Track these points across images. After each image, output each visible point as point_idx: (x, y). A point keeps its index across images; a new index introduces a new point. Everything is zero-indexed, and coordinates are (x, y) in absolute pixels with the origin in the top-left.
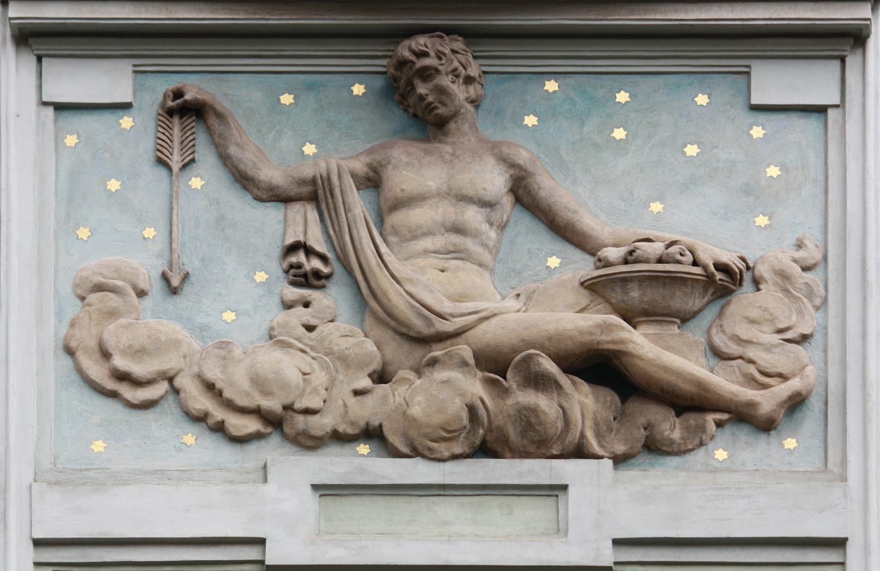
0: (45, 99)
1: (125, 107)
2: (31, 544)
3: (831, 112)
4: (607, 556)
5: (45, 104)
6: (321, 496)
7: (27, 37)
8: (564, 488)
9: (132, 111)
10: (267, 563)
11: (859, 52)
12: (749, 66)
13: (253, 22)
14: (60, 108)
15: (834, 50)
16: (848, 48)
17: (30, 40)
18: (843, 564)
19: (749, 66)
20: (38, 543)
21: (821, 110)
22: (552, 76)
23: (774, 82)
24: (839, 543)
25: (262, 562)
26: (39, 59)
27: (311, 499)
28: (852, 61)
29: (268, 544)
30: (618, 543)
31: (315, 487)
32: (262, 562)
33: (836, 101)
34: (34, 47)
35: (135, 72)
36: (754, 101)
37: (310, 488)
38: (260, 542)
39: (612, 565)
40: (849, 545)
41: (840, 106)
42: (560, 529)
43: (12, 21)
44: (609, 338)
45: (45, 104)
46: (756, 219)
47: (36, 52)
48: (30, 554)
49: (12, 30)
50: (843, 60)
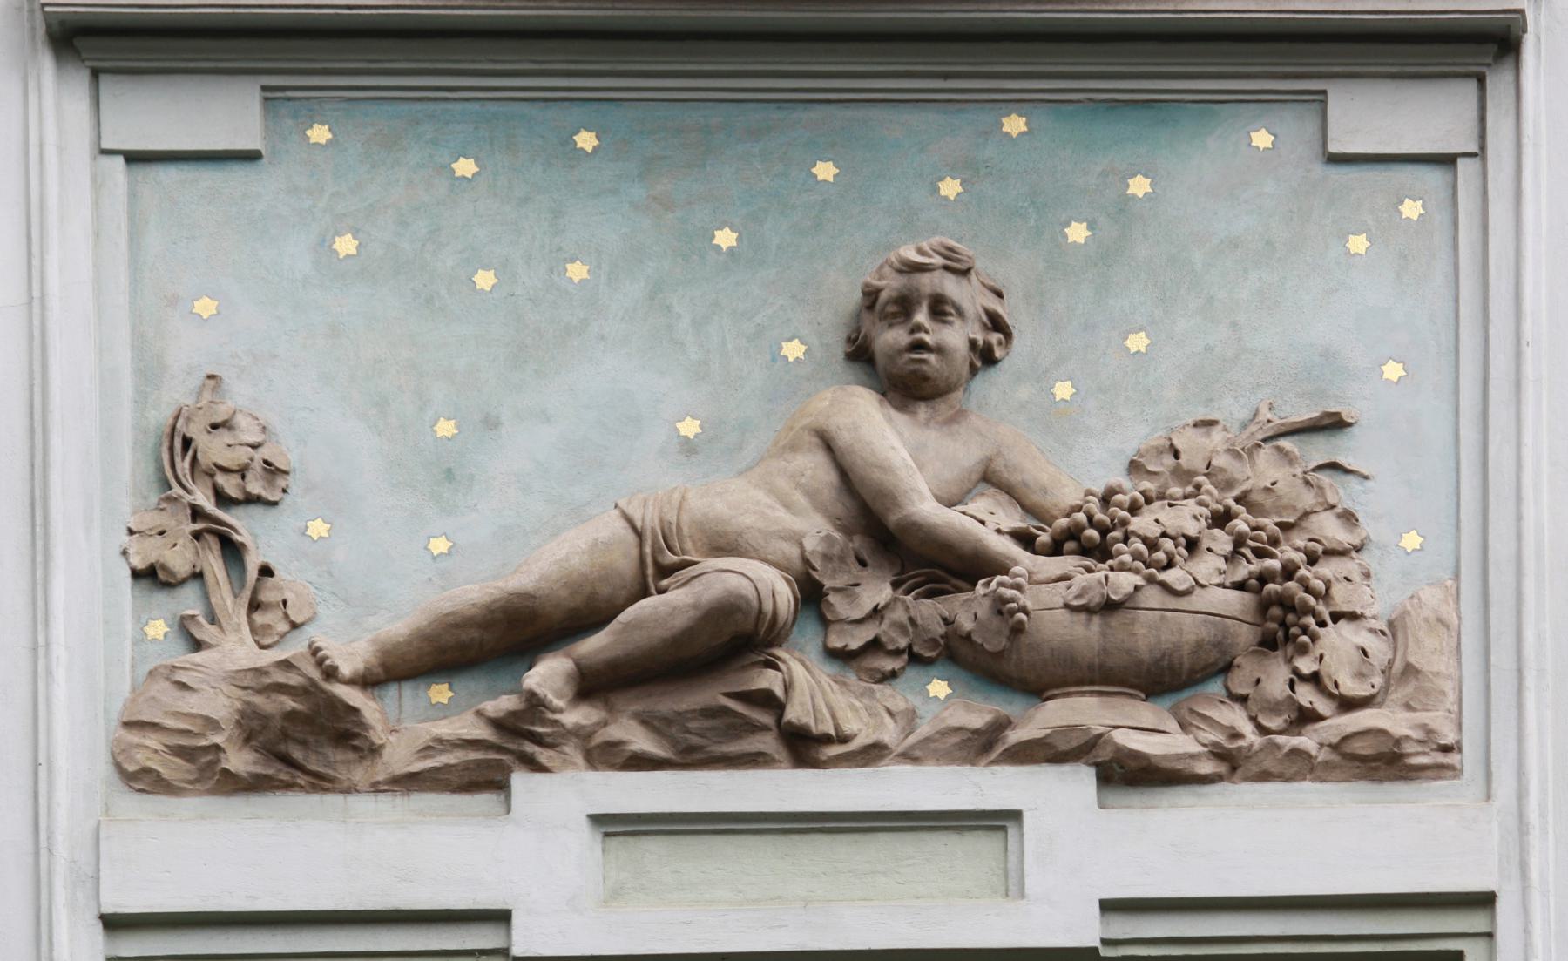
0: (106, 145)
1: (251, 157)
2: (100, 926)
3: (1461, 162)
4: (1087, 931)
5: (105, 152)
6: (607, 835)
7: (76, 41)
8: (1016, 816)
9: (265, 161)
10: (518, 950)
11: (1510, 61)
12: (1324, 92)
13: (469, 12)
14: (134, 158)
15: (1455, 64)
16: (1489, 60)
17: (79, 42)
18: (1490, 935)
19: (1324, 92)
20: (114, 924)
21: (1447, 161)
22: (1012, 105)
23: (1370, 115)
24: (1485, 901)
25: (505, 952)
26: (95, 74)
27: (586, 839)
28: (1498, 82)
29: (516, 920)
30: (1109, 907)
31: (597, 820)
32: (505, 952)
33: (1473, 148)
34: (84, 56)
35: (266, 99)
36: (1334, 148)
37: (585, 824)
38: (501, 917)
39: (1097, 944)
40: (1501, 905)
41: (1480, 154)
42: (1012, 885)
43: (47, 9)
44: (1421, 634)
45: (105, 152)
46: (569, 266)
47: (88, 63)
48: (95, 940)
49: (49, 26)
50: (1481, 80)
